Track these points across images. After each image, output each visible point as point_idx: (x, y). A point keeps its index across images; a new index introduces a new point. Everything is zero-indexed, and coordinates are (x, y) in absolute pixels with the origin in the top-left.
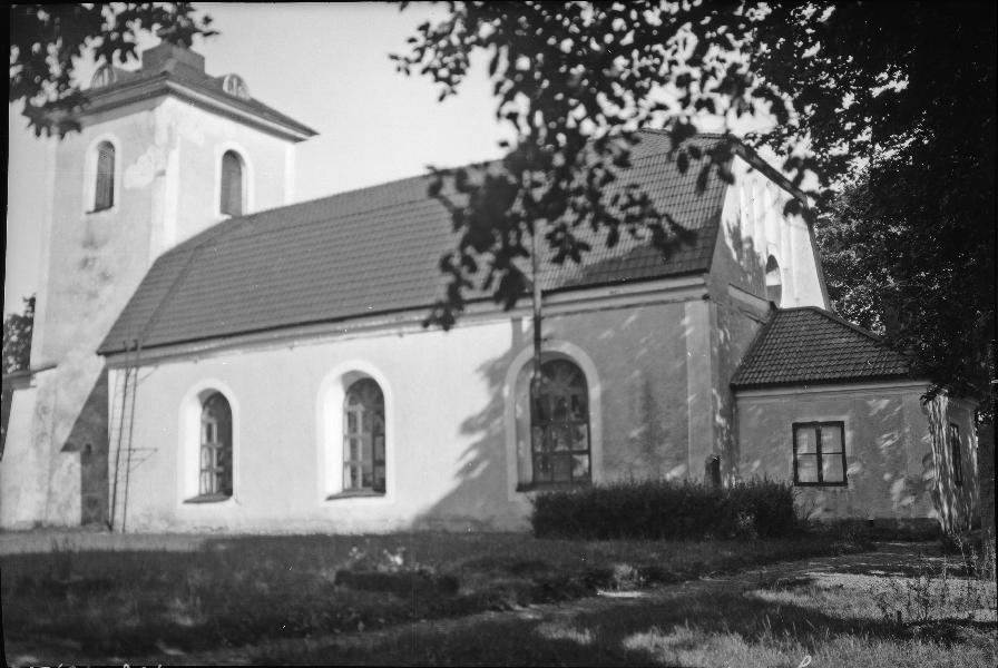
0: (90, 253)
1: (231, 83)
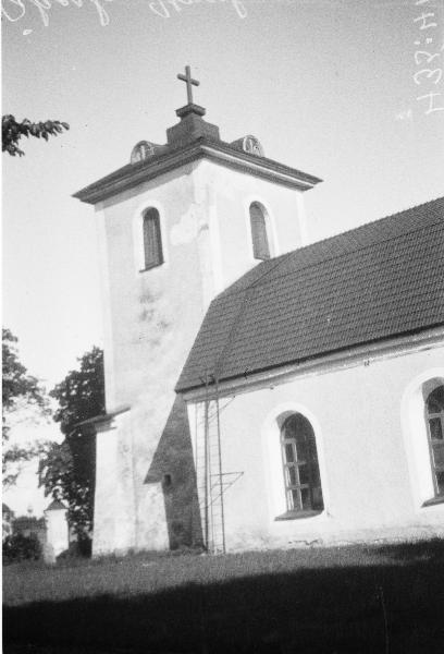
0: (148, 306)
1: (248, 143)
